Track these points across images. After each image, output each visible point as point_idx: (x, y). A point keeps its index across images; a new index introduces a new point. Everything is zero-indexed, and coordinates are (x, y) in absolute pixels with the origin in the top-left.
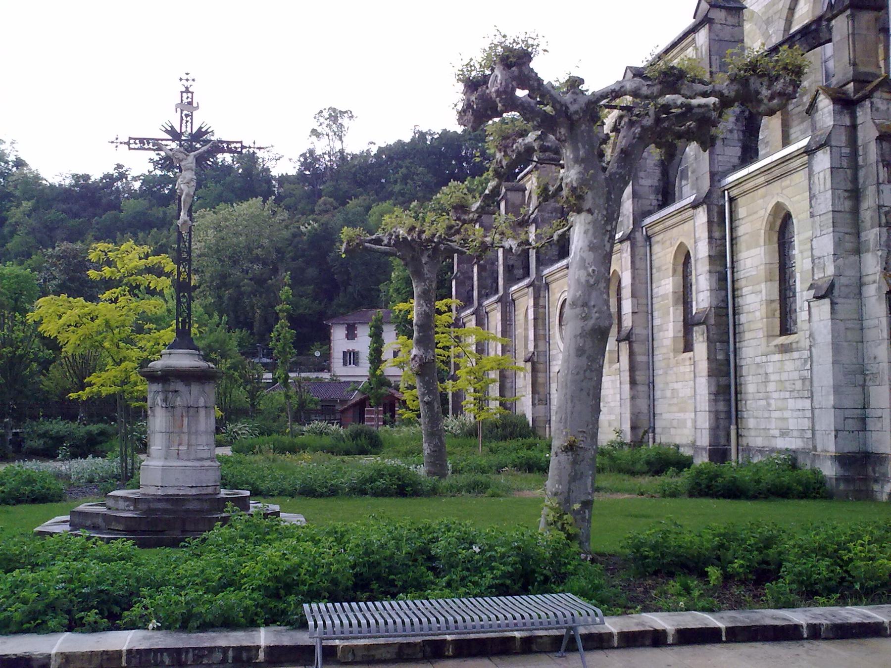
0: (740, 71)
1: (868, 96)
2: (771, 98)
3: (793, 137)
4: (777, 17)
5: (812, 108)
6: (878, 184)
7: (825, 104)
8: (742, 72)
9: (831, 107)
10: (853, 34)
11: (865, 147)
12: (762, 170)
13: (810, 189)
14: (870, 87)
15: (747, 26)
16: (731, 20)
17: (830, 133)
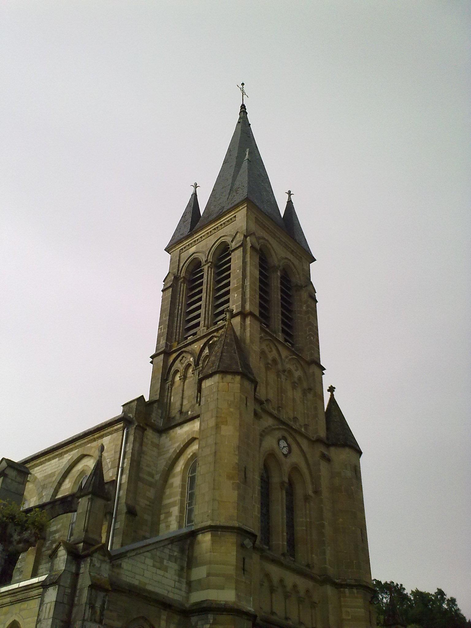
0: (3, 516)
1: (90, 555)
2: (19, 542)
3: (40, 571)
4: (51, 485)
5: (53, 555)
6: (84, 620)
7: (62, 553)
8: (5, 518)
9: (66, 557)
10: (90, 511)
11: (82, 590)
12: (10, 592)
13: (39, 615)
14: (93, 549)
15: (29, 486)
16: (19, 479)
17: (61, 575)
